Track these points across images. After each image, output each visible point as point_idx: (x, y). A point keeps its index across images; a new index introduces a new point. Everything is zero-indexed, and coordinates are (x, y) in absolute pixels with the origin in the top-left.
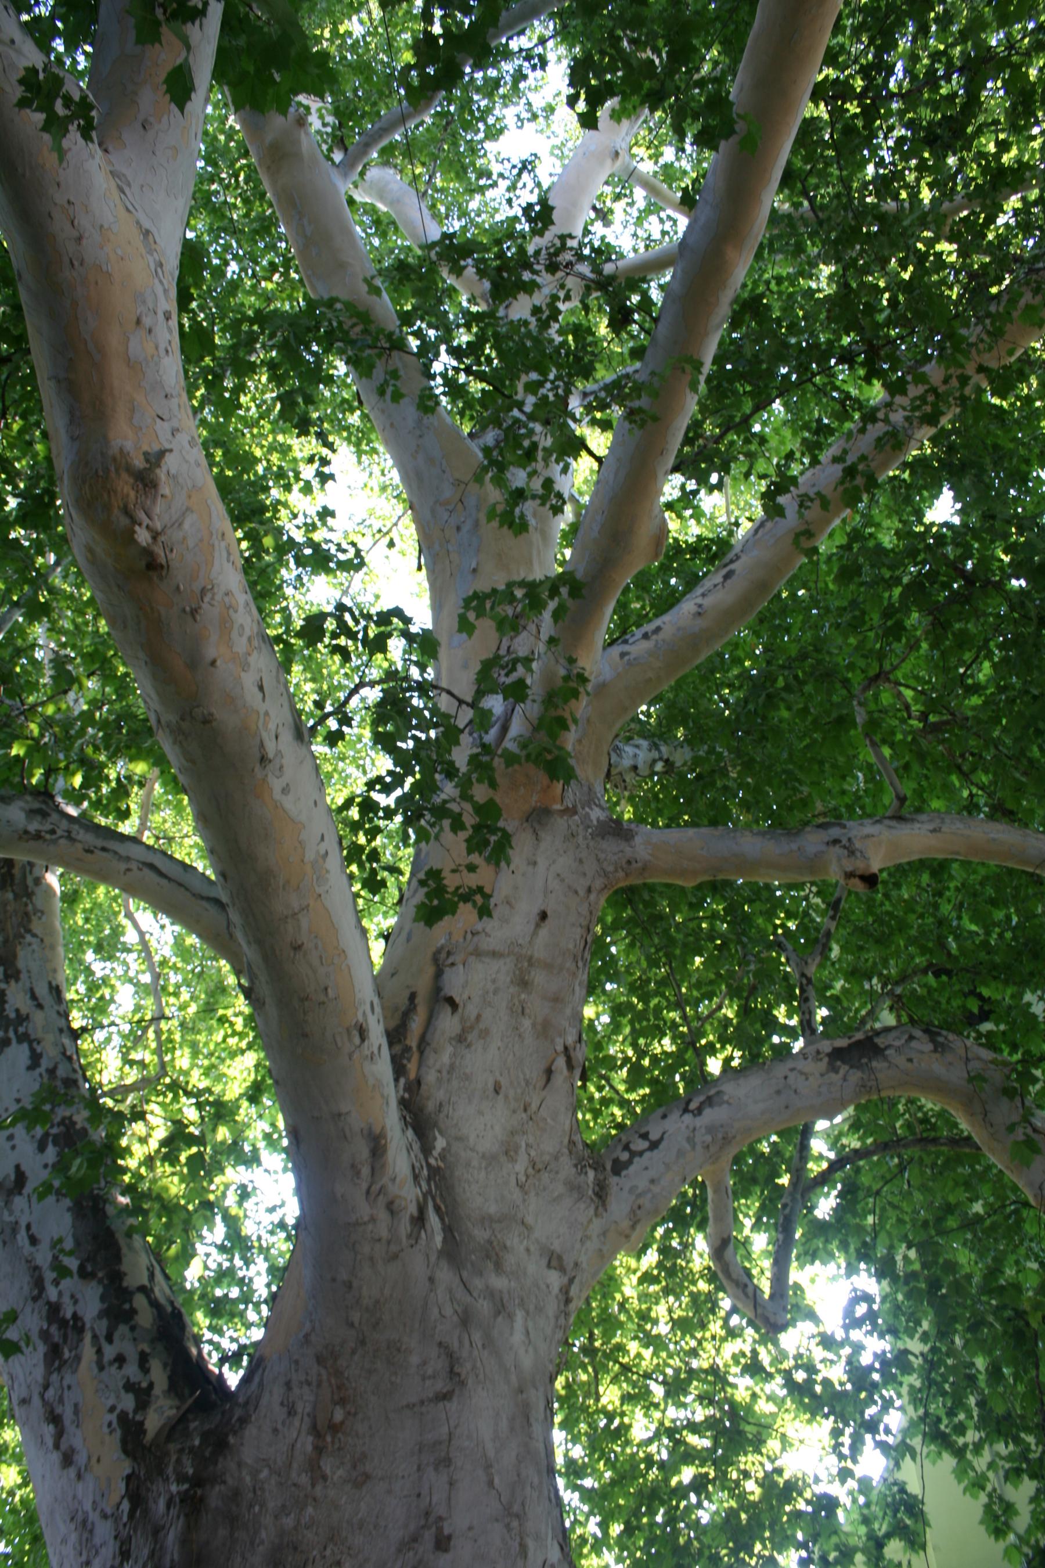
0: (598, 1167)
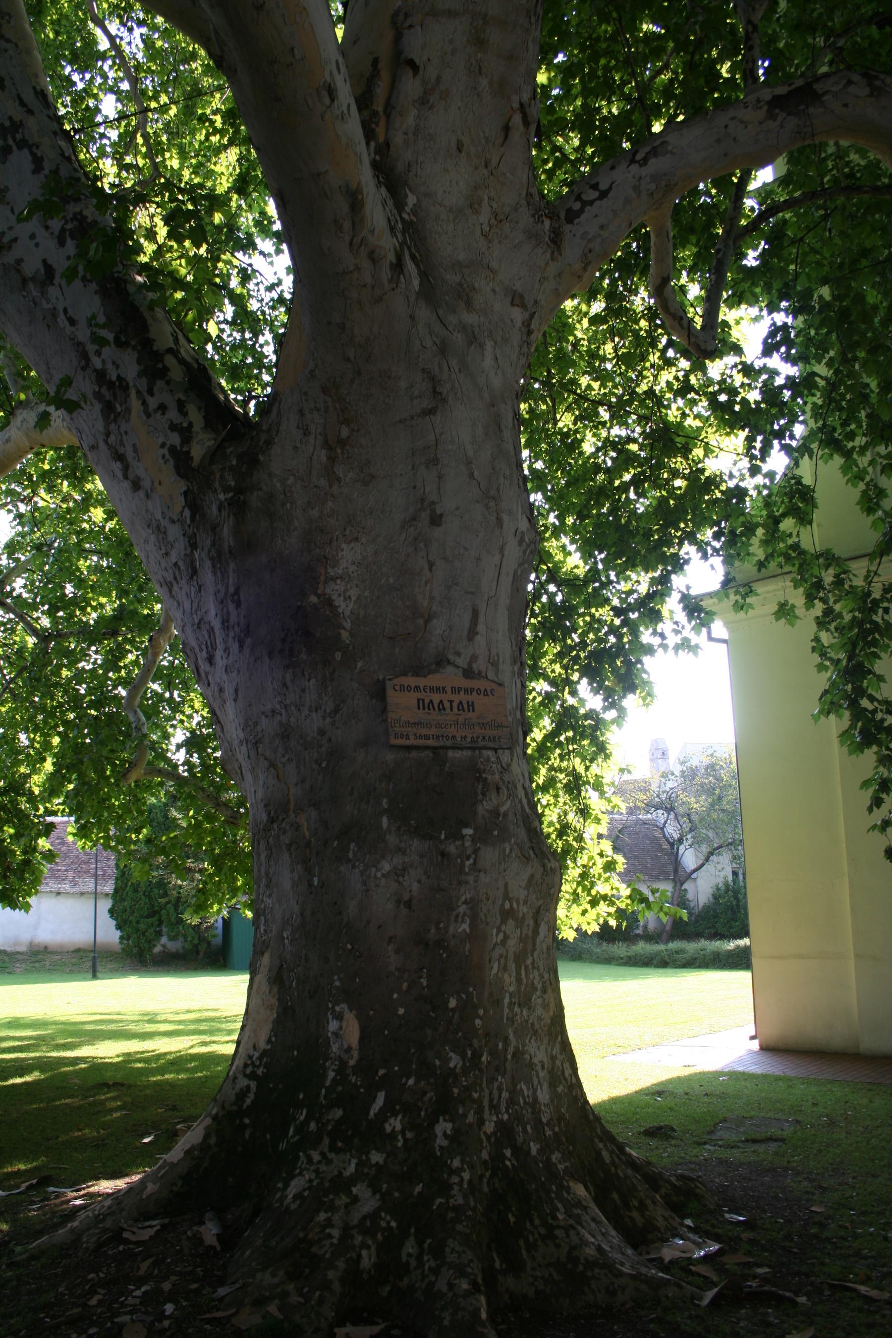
0: (553, 215)
